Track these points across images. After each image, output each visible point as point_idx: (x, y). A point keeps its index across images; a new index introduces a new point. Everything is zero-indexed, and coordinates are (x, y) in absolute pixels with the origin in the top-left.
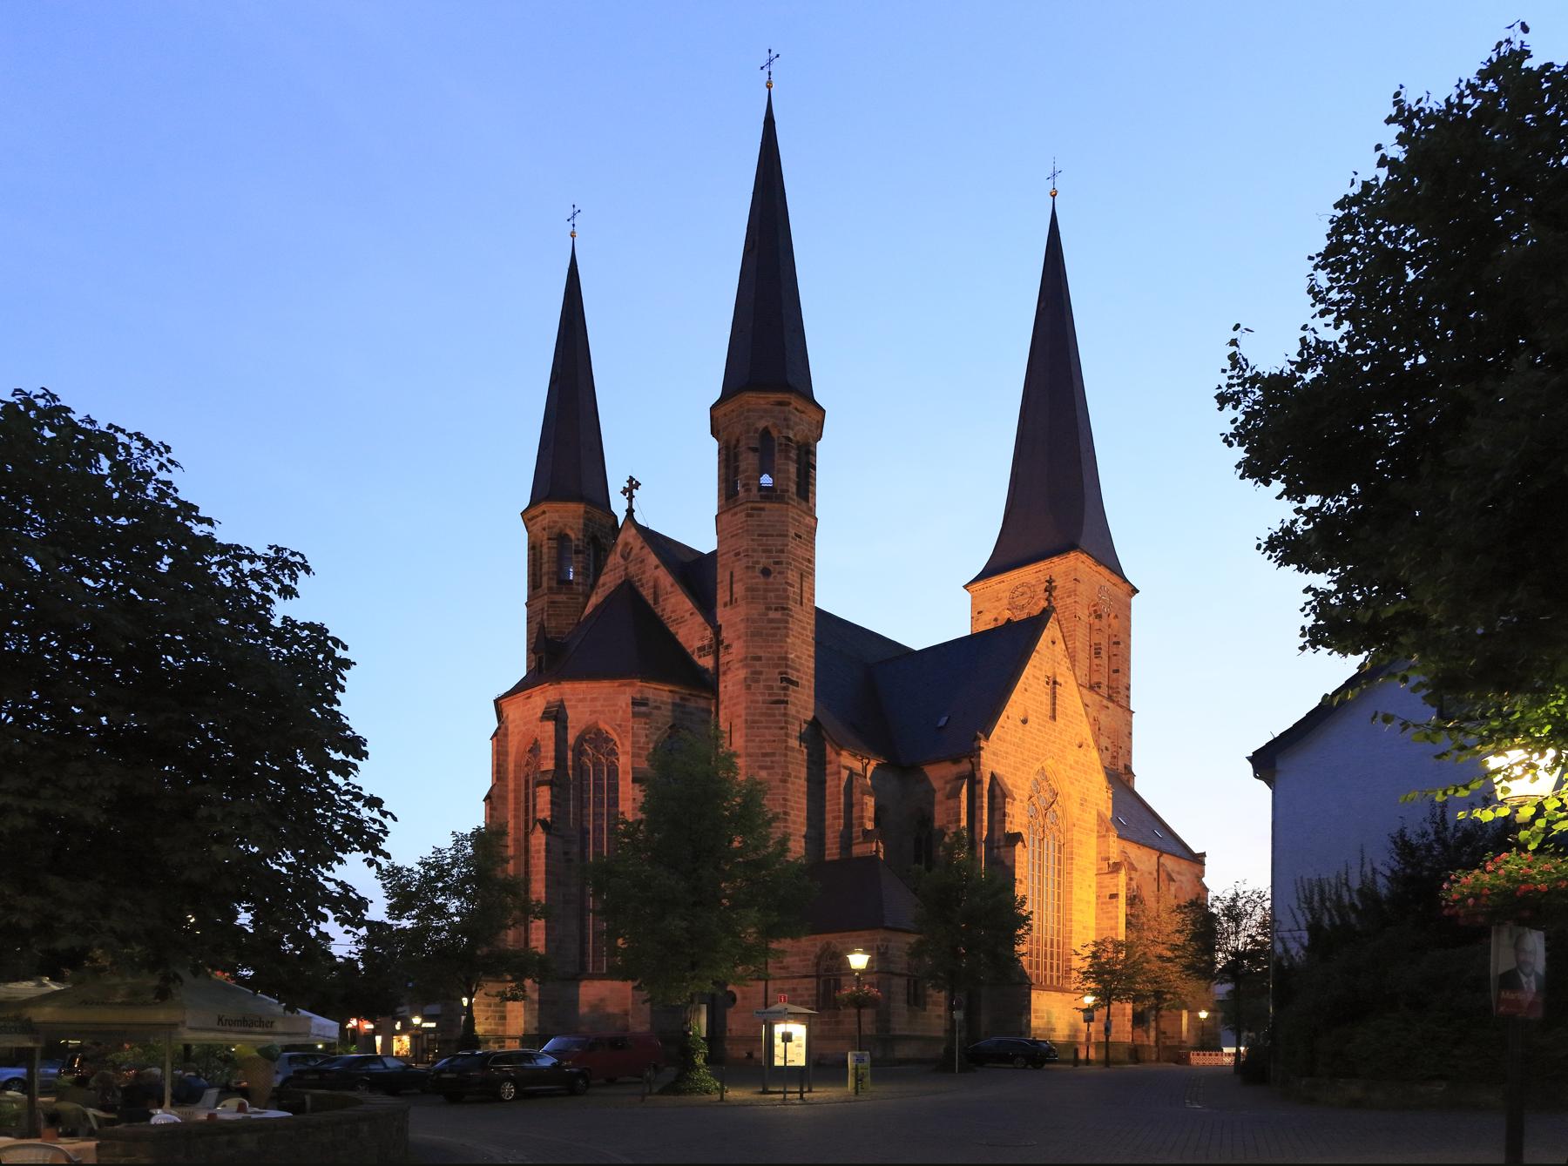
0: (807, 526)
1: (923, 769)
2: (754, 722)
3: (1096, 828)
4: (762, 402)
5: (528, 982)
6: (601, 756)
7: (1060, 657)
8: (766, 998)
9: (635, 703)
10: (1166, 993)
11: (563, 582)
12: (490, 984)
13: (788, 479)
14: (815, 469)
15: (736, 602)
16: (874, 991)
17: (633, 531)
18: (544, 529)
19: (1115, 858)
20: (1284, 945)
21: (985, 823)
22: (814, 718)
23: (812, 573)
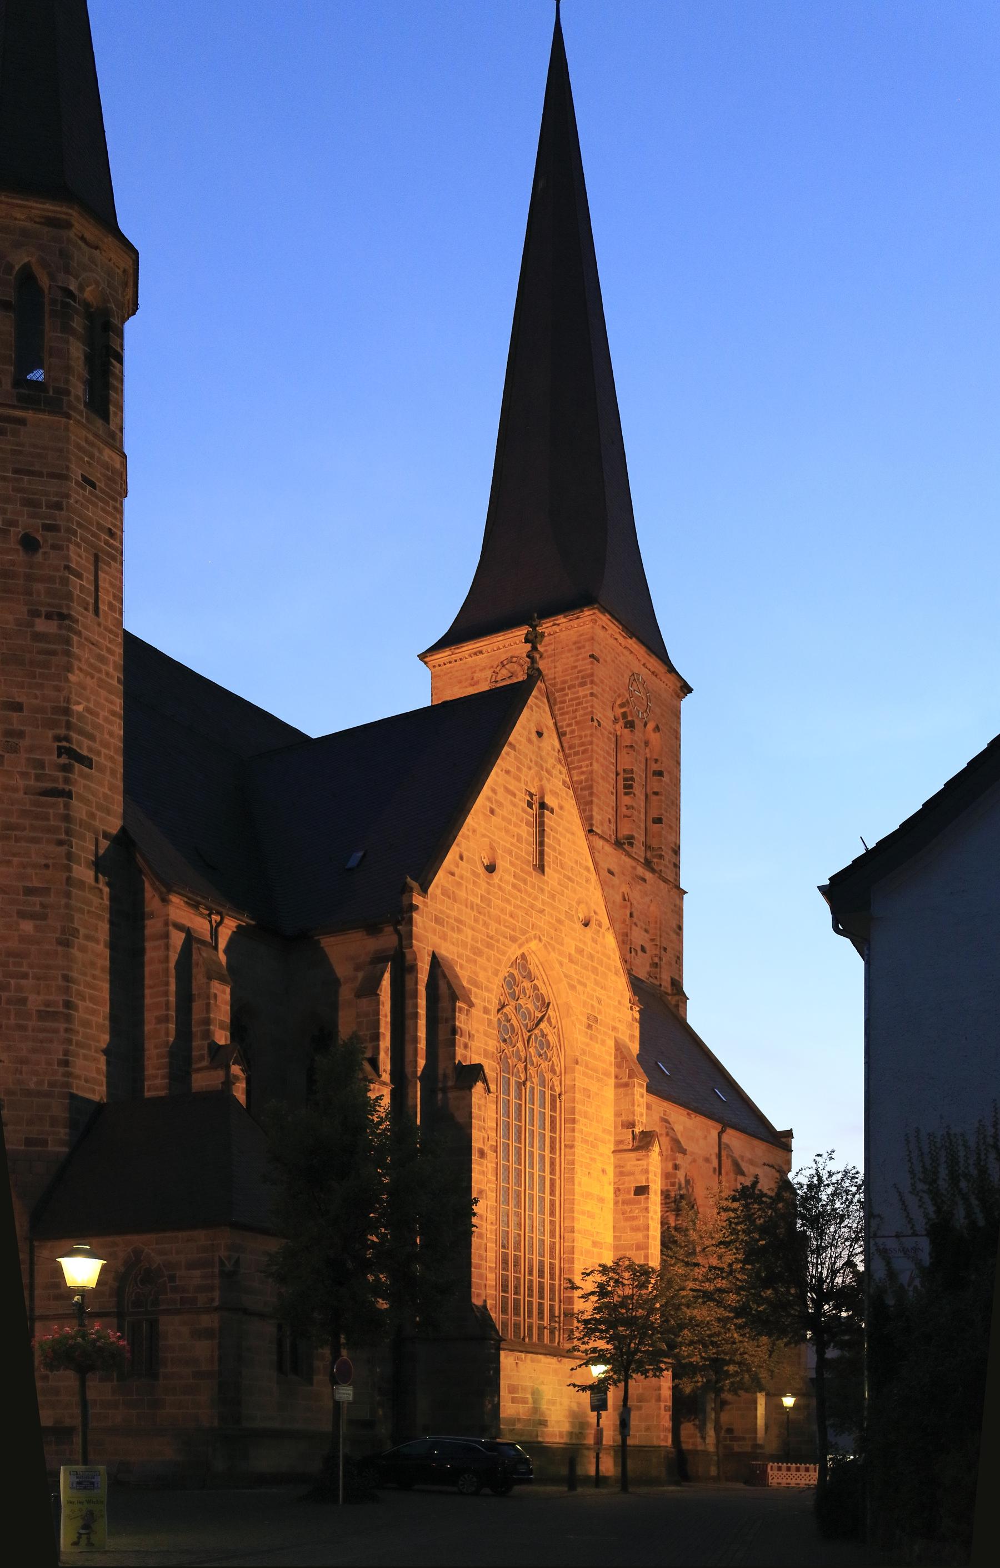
0: (106, 466)
1: (318, 942)
3: (612, 1070)
4: (19, 216)
7: (552, 761)
10: (729, 1363)
13: (68, 369)
19: (644, 1121)
20: (888, 1264)
21: (422, 1045)
22: (123, 830)
23: (116, 556)
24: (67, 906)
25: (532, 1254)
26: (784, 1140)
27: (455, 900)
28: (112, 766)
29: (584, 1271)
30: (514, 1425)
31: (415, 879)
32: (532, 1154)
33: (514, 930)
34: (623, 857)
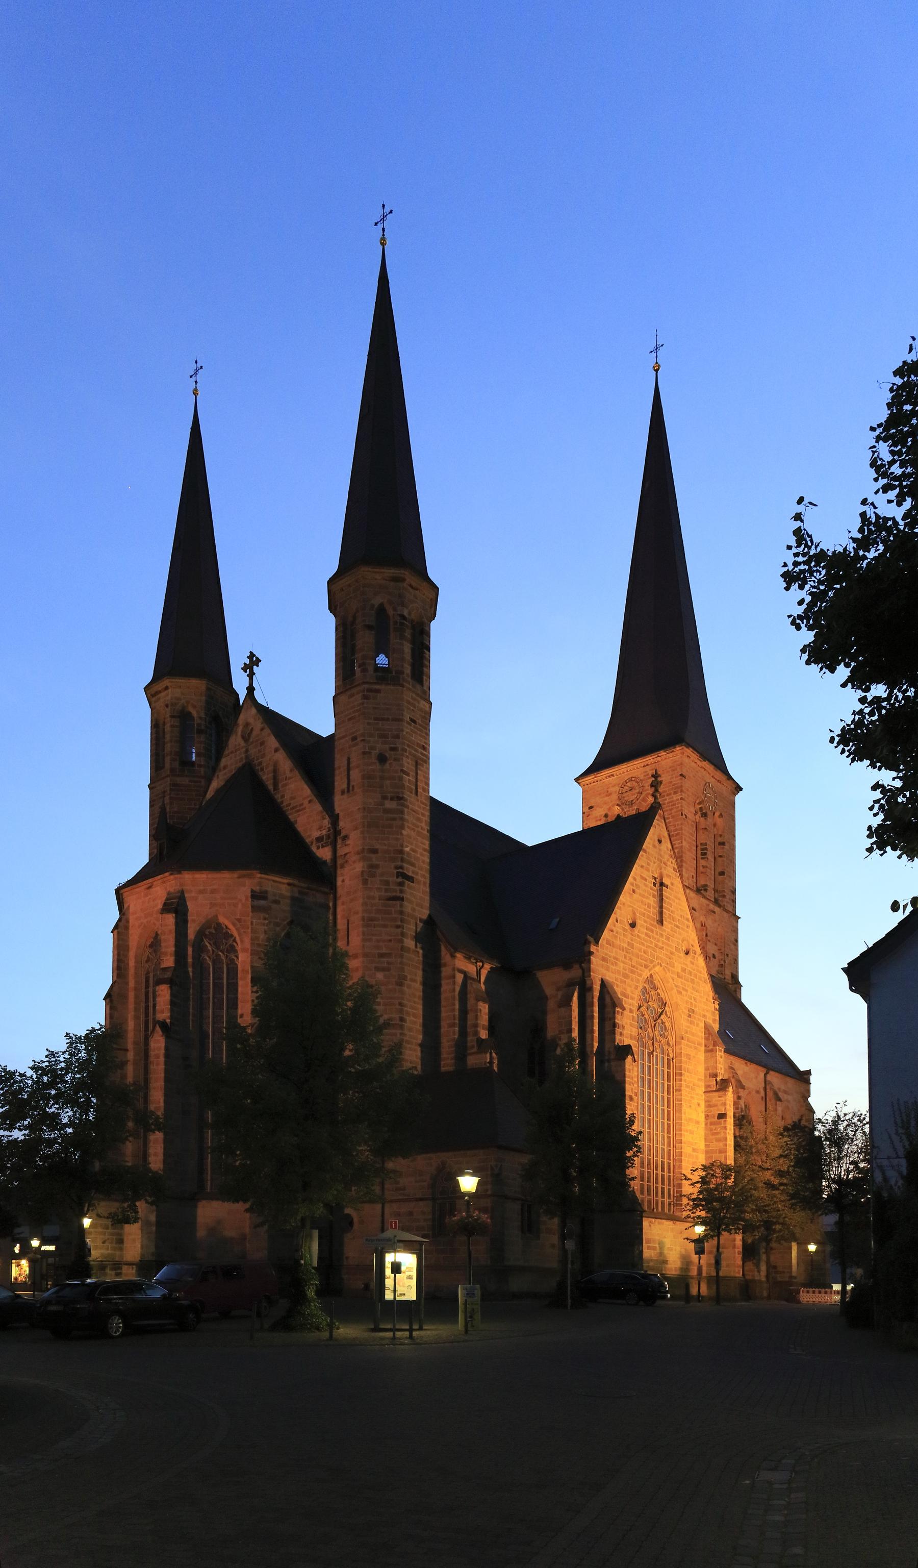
0: (421, 710)
1: (535, 974)
2: (372, 919)
3: (703, 1041)
5: (141, 1205)
6: (220, 953)
7: (666, 857)
8: (383, 1222)
9: (255, 896)
10: (775, 1223)
11: (186, 763)
12: (103, 1203)
14: (429, 651)
15: (353, 790)
16: (485, 1217)
17: (254, 711)
18: (167, 706)
19: (722, 1074)
20: (883, 1173)
21: (596, 1034)
22: (430, 916)
24: (401, 963)
25: (658, 1158)
26: (805, 1076)
27: (613, 947)
28: (424, 880)
29: (692, 1169)
30: (649, 1263)
31: (591, 936)
32: (657, 1095)
33: (646, 961)
34: (701, 899)
